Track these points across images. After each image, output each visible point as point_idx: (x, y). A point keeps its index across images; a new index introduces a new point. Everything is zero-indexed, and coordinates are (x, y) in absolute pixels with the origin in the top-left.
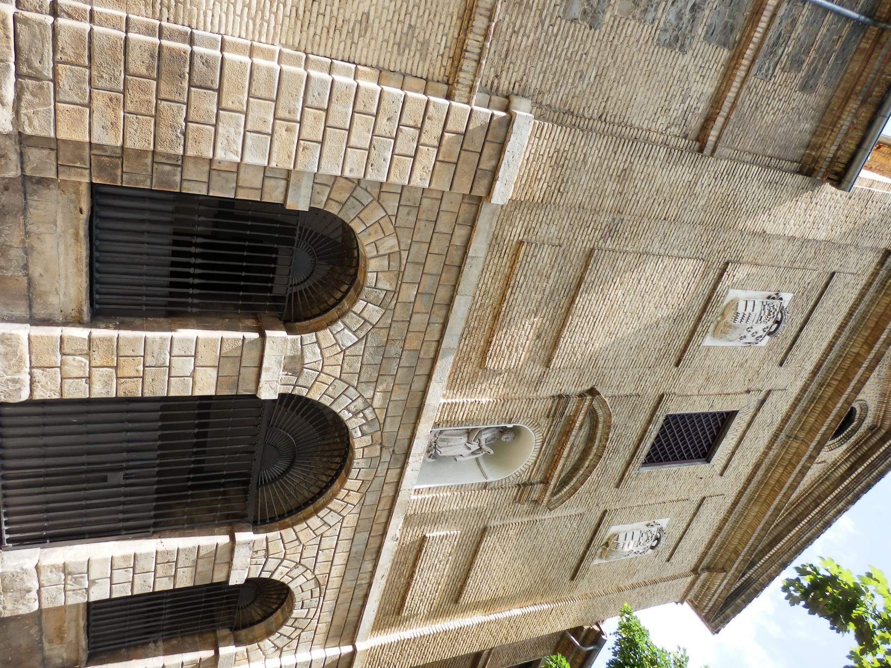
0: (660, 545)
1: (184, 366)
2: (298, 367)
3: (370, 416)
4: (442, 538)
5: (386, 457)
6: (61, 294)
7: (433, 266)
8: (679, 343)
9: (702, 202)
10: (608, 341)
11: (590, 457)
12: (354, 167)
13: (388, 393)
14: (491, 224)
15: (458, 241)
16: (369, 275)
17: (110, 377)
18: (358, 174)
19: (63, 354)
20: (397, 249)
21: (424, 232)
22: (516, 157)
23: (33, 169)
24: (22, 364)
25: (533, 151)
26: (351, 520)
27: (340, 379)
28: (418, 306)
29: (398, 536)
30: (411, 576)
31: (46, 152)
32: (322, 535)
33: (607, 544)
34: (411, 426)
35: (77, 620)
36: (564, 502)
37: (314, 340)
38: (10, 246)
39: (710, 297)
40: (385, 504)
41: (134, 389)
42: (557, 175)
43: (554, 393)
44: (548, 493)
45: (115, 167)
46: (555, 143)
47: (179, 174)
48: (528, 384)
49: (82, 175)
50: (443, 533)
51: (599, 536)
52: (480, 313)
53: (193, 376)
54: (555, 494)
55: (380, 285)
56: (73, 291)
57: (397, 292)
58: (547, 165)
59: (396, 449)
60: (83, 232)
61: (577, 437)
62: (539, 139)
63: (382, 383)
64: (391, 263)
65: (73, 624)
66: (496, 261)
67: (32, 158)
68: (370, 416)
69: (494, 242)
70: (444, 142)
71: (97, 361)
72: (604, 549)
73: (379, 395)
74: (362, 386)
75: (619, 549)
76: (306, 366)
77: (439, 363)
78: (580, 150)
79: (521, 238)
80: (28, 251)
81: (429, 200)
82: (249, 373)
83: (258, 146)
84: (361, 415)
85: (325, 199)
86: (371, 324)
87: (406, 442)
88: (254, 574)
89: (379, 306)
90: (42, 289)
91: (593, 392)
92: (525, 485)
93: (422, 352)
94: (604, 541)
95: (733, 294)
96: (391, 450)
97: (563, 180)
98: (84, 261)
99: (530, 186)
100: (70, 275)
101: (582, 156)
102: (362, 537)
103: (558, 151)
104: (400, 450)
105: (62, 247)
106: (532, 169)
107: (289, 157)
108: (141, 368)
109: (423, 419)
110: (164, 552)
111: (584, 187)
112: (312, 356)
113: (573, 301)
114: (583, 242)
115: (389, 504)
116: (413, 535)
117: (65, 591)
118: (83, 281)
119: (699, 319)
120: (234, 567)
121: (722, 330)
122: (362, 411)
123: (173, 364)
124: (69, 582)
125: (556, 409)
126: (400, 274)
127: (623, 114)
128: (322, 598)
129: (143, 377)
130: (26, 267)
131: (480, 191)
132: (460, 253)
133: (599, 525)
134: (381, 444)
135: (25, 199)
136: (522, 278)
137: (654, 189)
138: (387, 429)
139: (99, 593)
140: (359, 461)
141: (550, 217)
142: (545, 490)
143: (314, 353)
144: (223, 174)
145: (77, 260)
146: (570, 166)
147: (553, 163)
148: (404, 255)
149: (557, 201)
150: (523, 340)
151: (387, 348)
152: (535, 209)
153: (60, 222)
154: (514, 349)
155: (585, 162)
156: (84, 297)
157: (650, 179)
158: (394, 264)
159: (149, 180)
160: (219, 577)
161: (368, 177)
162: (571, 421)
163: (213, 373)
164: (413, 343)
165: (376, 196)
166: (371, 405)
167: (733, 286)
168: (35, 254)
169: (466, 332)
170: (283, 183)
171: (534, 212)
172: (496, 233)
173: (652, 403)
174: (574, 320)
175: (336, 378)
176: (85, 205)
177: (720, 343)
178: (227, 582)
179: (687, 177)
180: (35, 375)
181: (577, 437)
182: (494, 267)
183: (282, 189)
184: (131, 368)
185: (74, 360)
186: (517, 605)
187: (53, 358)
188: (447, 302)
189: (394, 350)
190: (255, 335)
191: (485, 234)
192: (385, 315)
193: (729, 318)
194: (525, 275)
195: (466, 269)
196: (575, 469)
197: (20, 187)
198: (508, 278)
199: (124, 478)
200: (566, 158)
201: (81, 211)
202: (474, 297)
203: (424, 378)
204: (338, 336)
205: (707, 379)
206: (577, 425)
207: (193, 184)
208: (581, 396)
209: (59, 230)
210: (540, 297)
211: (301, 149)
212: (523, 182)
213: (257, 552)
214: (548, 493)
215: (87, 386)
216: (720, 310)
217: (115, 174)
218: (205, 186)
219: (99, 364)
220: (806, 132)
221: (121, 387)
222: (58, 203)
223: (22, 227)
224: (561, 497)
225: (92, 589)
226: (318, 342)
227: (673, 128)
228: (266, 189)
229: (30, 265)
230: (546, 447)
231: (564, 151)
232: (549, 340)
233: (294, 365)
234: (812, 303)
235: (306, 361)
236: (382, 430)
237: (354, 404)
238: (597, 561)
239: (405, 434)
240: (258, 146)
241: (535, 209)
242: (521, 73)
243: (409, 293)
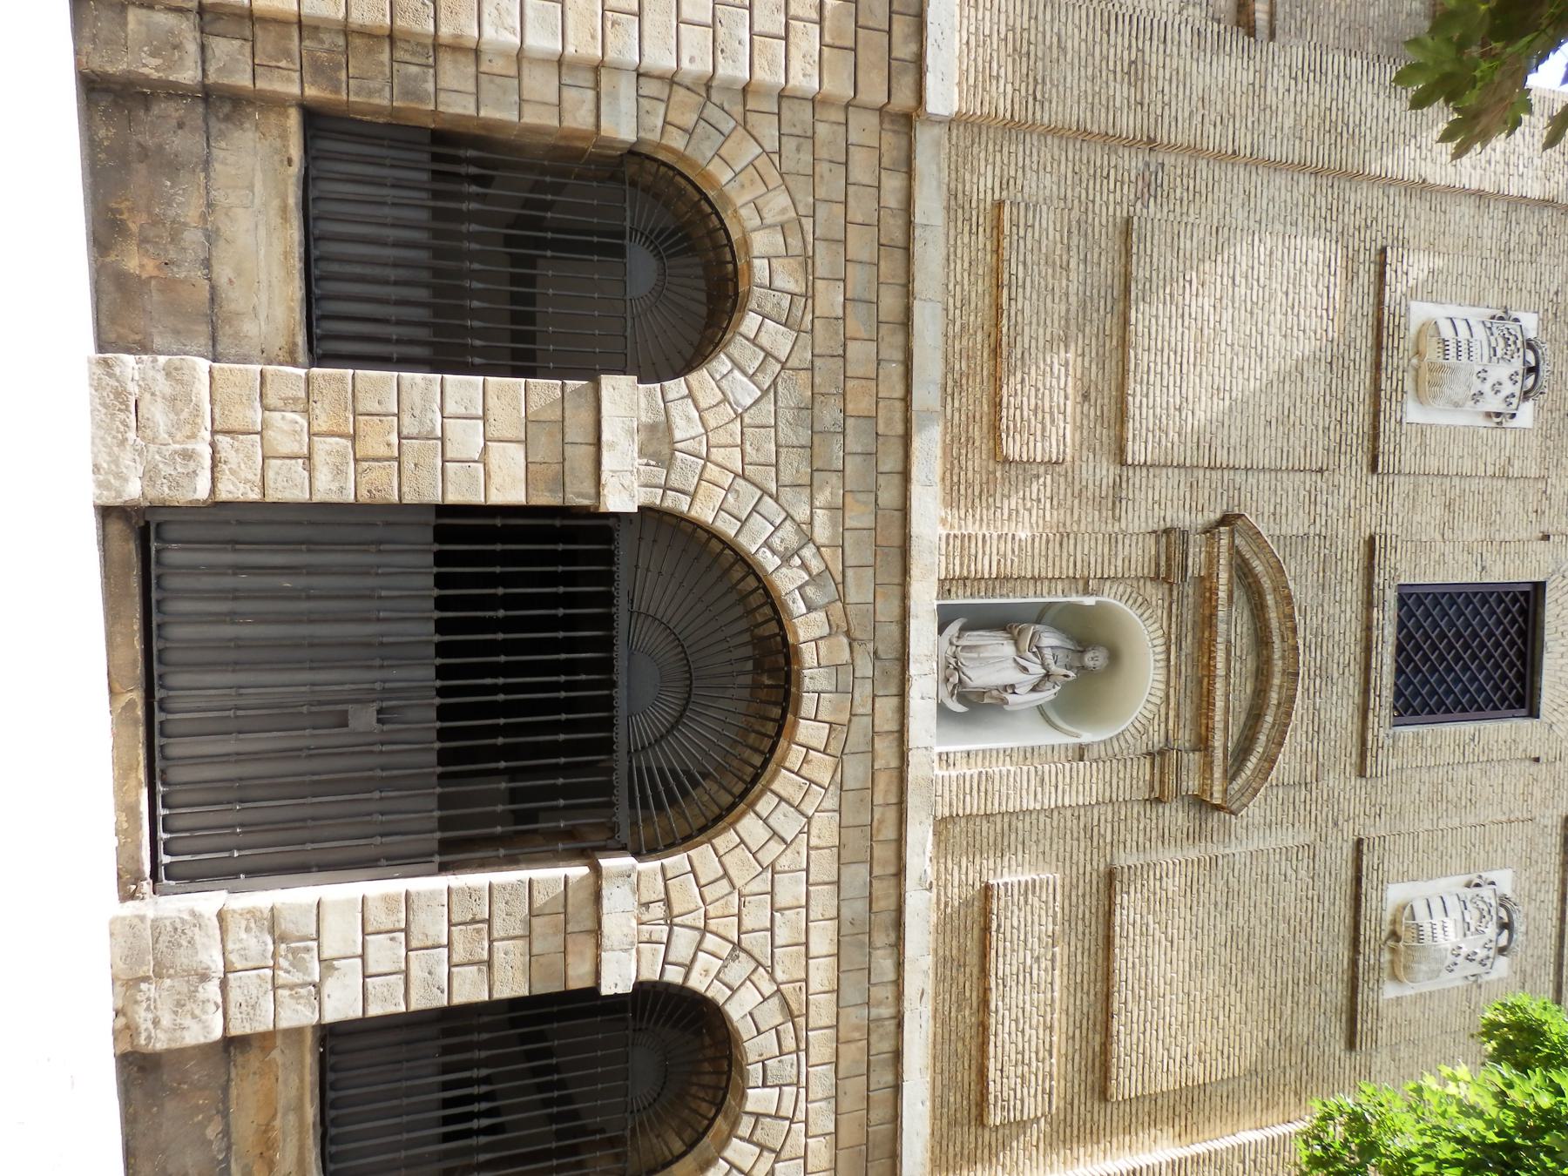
0: (1519, 937)
1: (467, 439)
2: (666, 451)
3: (816, 565)
4: (1029, 889)
5: (865, 667)
6: (262, 317)
7: (861, 245)
8: (1359, 418)
9: (1289, 122)
10: (1221, 406)
11: (1276, 681)
12: (696, 53)
13: (837, 510)
14: (938, 164)
15: (892, 200)
16: (757, 262)
17: (344, 456)
18: (703, 66)
19: (265, 408)
21: (831, 184)
22: (947, 32)
23: (219, 70)
24: (199, 421)
25: (972, 29)
26: (825, 829)
27: (743, 477)
28: (855, 326)
29: (931, 876)
30: (984, 1002)
31: (237, 43)
32: (773, 864)
33: (1394, 935)
34: (897, 590)
35: (299, 1109)
36: (1256, 791)
38: (185, 224)
39: (1379, 321)
40: (884, 791)
41: (384, 486)
42: (1024, 71)
43: (1152, 526)
44: (1218, 773)
45: (337, 67)
46: (1003, 17)
47: (431, 80)
48: (1098, 502)
49: (289, 80)
50: (1027, 877)
51: (1367, 930)
52: (964, 342)
53: (483, 458)
54: (1233, 778)
56: (280, 313)
57: (810, 295)
58: (1003, 53)
59: (881, 649)
60: (293, 198)
61: (1233, 625)
62: (977, 9)
63: (821, 488)
64: (789, 240)
65: (292, 1117)
66: (966, 240)
67: (217, 52)
68: (816, 565)
69: (953, 203)
70: (827, 13)
71: (322, 424)
72: (1393, 951)
73: (821, 516)
74: (787, 494)
75: (1427, 941)
76: (678, 446)
77: (917, 443)
78: (1048, 28)
79: (997, 196)
80: (211, 236)
81: (827, 126)
82: (579, 456)
83: (544, 19)
84: (797, 561)
85: (660, 123)
86: (777, 360)
87: (895, 630)
88: (651, 974)
89: (785, 325)
90: (233, 306)
91: (1227, 520)
92: (1161, 753)
93: (880, 422)
94: (1387, 927)
96: (870, 646)
97: (1035, 80)
98: (297, 251)
99: (984, 89)
100: (275, 282)
101: (1055, 39)
102: (857, 875)
103: (1013, 29)
104: (888, 651)
105: (262, 232)
106: (980, 60)
107: (593, 37)
108: (394, 439)
109: (915, 571)
110: (462, 889)
111: (1076, 92)
112: (685, 427)
113: (1126, 322)
115: (894, 789)
116: (966, 876)
117: (275, 988)
118: (296, 289)
119: (1377, 366)
120: (606, 942)
121: (1428, 383)
122: (797, 552)
123: (449, 434)
124: (283, 962)
125: (1168, 559)
129: (399, 459)
130: (207, 264)
131: (903, 99)
132: (900, 222)
133: (1358, 880)
134: (847, 633)
135: (208, 146)
136: (1021, 267)
137: (1194, 97)
138: (852, 597)
139: (342, 1004)
140: (814, 677)
141: (1035, 158)
142: (1208, 766)
143: (689, 419)
144: (498, 80)
145: (286, 254)
146: (1040, 54)
147: (1010, 50)
148: (808, 224)
150: (1058, 398)
151: (816, 411)
152: (1006, 143)
153: (258, 187)
154: (1047, 416)
155: (1062, 49)
156: (298, 317)
157: (1180, 78)
158: (795, 243)
159: (387, 89)
161: (720, 71)
162: (1206, 587)
163: (517, 452)
164: (860, 404)
165: (740, 119)
166: (811, 540)
167: (1412, 293)
168: (222, 243)
169: (950, 383)
170: (591, 94)
171: (1005, 150)
172: (952, 186)
173: (1359, 558)
174: (1140, 358)
175: (736, 475)
176: (295, 151)
177: (1408, 991)
179: (1246, 77)
180: (219, 447)
182: (966, 251)
183: (589, 105)
184: (379, 440)
185: (283, 418)
186: (1247, 1121)
187: (250, 413)
188: (901, 318)
189: (829, 415)
190: (584, 870)
191: (934, 184)
192: (799, 343)
193: (1432, 353)
194: (1025, 263)
195: (918, 248)
196: (1255, 716)
197: (200, 122)
198: (997, 272)
199: (379, 721)
200: (1029, 43)
201: (290, 162)
202: (947, 310)
203: (897, 479)
204: (724, 383)
205: (1448, 506)
206: (1222, 594)
207: (454, 95)
208: (1210, 530)
209: (257, 201)
210: (1063, 308)
211: (609, 24)
212: (971, 81)
213: (647, 905)
214: (1218, 773)
215: (306, 474)
216: (1408, 344)
217: (338, 80)
219: (324, 428)
220: (1418, 14)
221: (363, 480)
222: (256, 154)
223: (203, 191)
224: (1248, 783)
225: (330, 987)
226: (691, 395)
227: (1191, 9)
228: (565, 105)
229: (214, 262)
230: (1178, 657)
231: (1023, 30)
232: (1106, 400)
233: (658, 442)
235: (678, 435)
236: (842, 598)
237: (780, 533)
238: (1390, 991)
239: (888, 610)
240: (544, 19)
241: (1006, 143)
243: (830, 299)
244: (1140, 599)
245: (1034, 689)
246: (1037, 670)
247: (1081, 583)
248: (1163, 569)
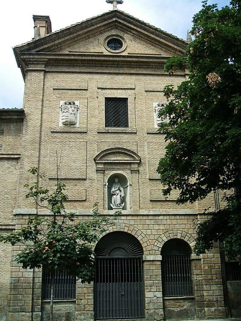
61: (113, 158)
92: (131, 171)
127: (14, 183)
128: (173, 230)
149: (10, 253)
181: (113, 158)
242: (9, 213)
245: (121, 191)
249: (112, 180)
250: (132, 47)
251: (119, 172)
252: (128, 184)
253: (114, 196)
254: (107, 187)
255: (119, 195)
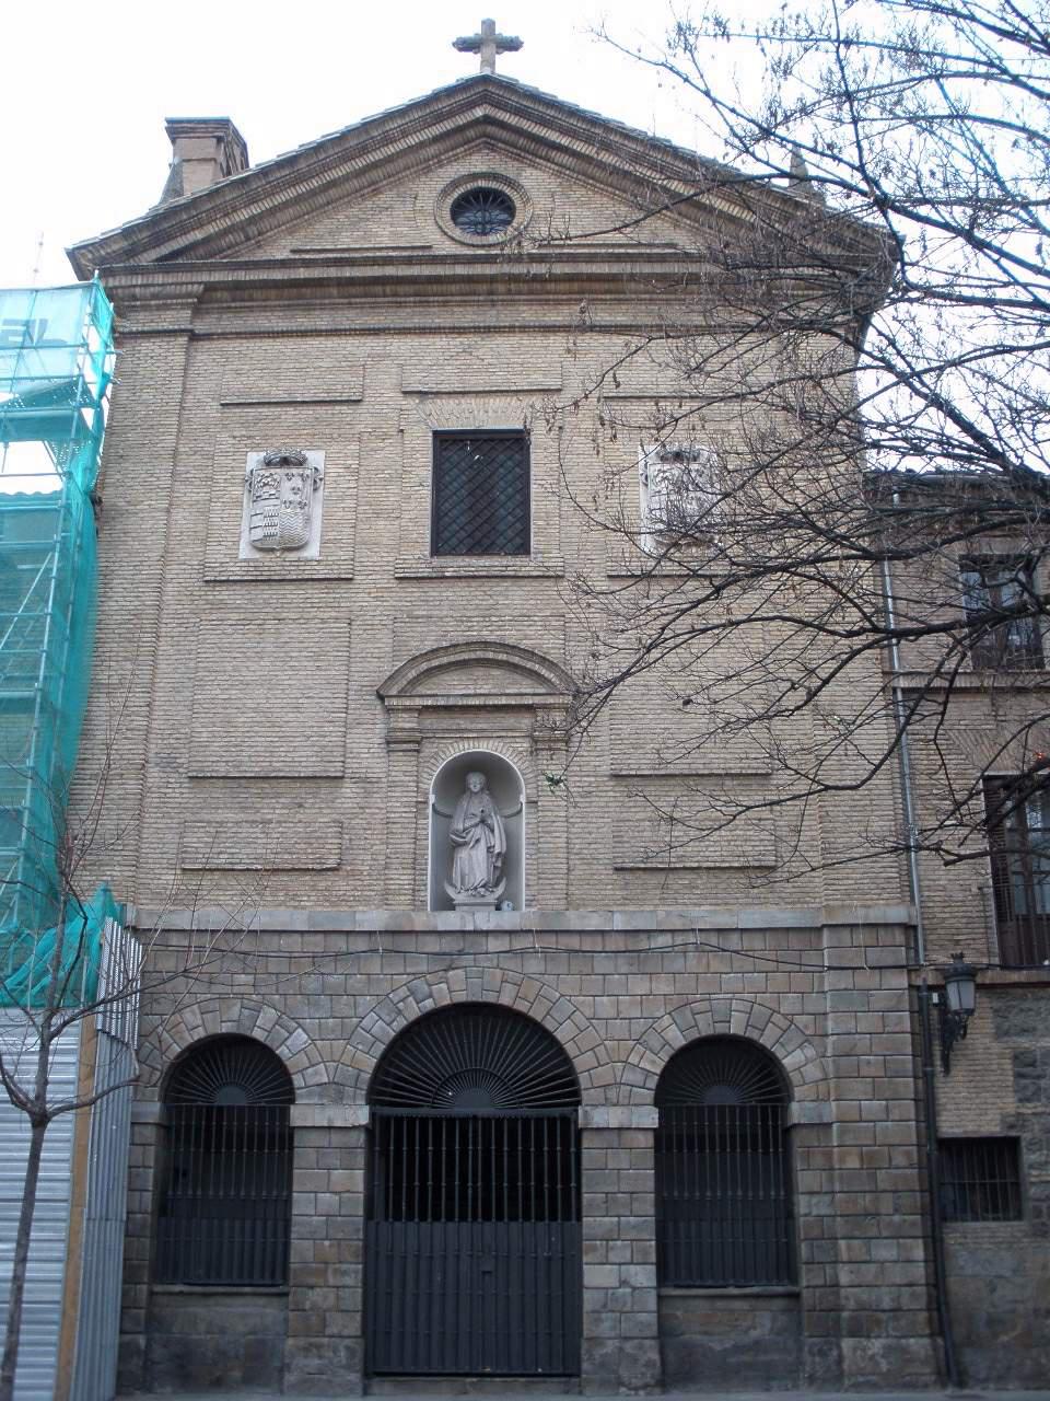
20: (195, 1007)
37: (300, 1075)
55: (236, 1018)
61: (456, 687)
95: (245, 552)
114: (180, 793)
126: (222, 998)
143: (316, 1073)
160: (647, 1141)
169: (292, 903)
178: (654, 1130)
181: (456, 687)
205: (378, 515)
218: (145, 1194)
233: (334, 1091)
234: (265, 410)
244: (433, 761)
245: (493, 831)
246: (478, 832)
247: (420, 806)
248: (412, 746)
249: (456, 778)
250: (556, 211)
251: (484, 747)
252: (523, 799)
253: (463, 854)
254: (430, 811)
255: (482, 846)
